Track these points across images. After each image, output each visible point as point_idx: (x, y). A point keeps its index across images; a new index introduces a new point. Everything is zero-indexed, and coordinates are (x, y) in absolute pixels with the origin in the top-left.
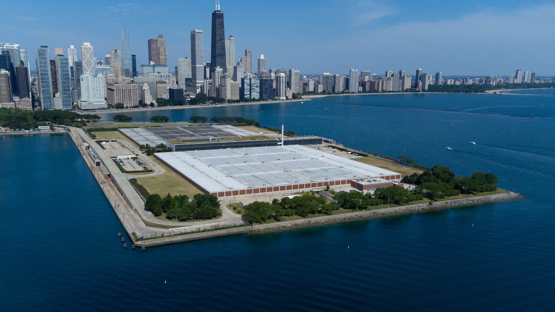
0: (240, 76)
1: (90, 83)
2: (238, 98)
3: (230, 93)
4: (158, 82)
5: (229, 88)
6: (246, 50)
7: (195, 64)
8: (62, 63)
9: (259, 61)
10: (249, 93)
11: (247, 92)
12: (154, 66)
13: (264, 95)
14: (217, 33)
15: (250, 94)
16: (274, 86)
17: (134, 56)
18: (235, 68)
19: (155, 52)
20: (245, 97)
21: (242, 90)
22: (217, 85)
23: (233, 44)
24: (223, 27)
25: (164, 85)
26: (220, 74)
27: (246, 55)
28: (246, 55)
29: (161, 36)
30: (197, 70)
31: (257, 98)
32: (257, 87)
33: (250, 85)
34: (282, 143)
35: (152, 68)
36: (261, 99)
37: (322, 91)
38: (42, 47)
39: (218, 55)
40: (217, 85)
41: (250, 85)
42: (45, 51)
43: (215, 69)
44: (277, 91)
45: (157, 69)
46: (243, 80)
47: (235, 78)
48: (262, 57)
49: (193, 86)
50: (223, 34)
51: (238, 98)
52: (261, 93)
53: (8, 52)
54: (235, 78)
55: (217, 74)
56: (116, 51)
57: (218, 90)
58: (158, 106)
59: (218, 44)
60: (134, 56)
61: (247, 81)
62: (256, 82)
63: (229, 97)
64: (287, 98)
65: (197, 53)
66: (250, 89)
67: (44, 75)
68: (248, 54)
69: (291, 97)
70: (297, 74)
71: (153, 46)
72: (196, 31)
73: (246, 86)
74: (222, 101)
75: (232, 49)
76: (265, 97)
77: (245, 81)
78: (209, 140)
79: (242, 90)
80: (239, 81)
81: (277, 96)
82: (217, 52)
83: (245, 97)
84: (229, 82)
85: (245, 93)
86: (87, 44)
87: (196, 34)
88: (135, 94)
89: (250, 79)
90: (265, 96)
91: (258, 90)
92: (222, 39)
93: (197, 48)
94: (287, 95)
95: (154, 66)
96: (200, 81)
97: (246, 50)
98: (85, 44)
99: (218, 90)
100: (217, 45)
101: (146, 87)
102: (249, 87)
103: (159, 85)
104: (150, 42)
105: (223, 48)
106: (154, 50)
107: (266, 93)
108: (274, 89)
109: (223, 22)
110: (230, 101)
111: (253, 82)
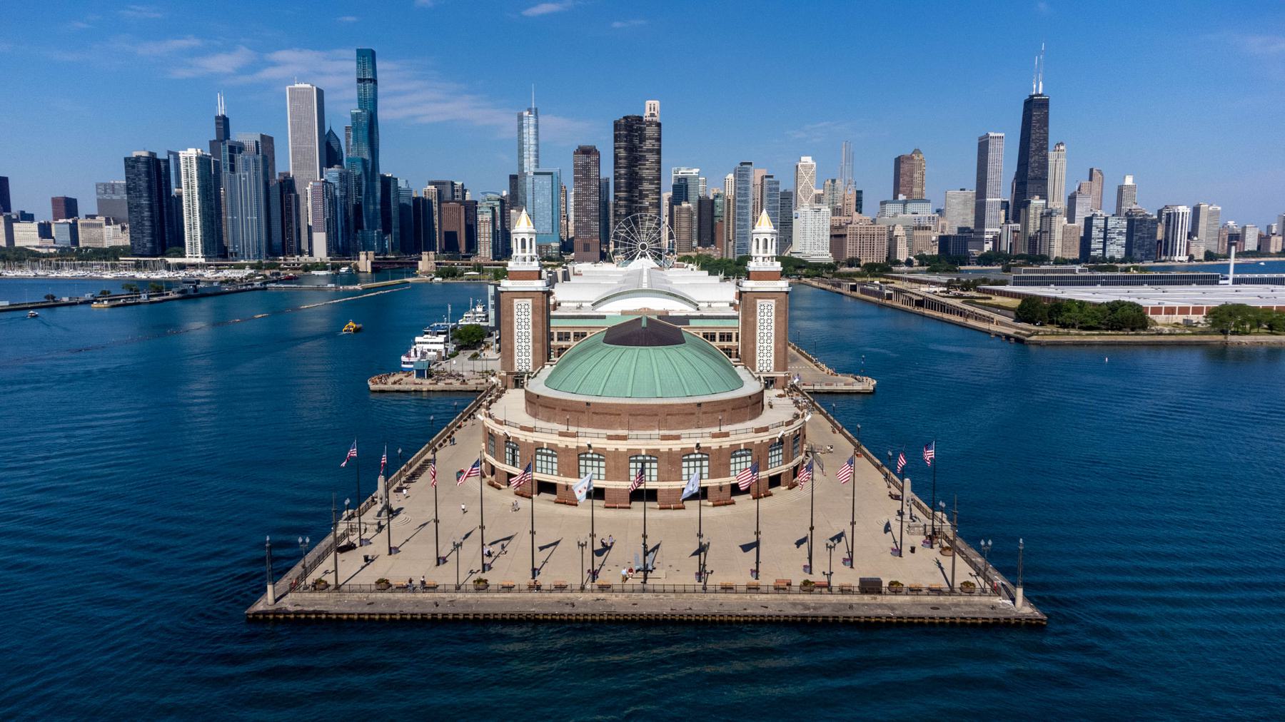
0: (1081, 213)
1: (809, 221)
2: (1077, 256)
3: (1060, 244)
4: (915, 228)
5: (1058, 235)
6: (1091, 170)
7: (985, 197)
8: (770, 189)
9: (1120, 190)
10: (1101, 246)
11: (1096, 245)
12: (905, 203)
13: (1134, 251)
14: (1033, 137)
15: (1104, 249)
16: (1160, 235)
17: (859, 193)
18: (1072, 199)
19: (907, 179)
20: (1093, 253)
21: (1086, 242)
22: (1031, 231)
23: (1063, 160)
24: (1047, 125)
25: (927, 233)
26: (1039, 211)
27: (1091, 179)
28: (1091, 179)
29: (917, 151)
30: (988, 208)
31: (1118, 256)
32: (1120, 233)
33: (1106, 230)
34: (1230, 281)
35: (900, 207)
36: (1129, 257)
37: (1279, 249)
38: (742, 164)
39: (1030, 177)
40: (1031, 231)
41: (1106, 230)
42: (747, 170)
43: (1029, 202)
44: (1167, 244)
45: (910, 207)
46: (1089, 222)
47: (1071, 217)
48: (1129, 181)
49: (977, 240)
50: (1046, 139)
51: (1077, 256)
52: (1129, 246)
53: (686, 179)
54: (1071, 217)
55: (1032, 211)
56: (834, 181)
57: (1033, 242)
58: (606, 479)
59: (1034, 160)
60: (859, 193)
61: (1098, 223)
62: (1119, 225)
63: (1057, 252)
64: (1191, 258)
65: (989, 176)
66: (1105, 238)
67: (742, 208)
68: (1096, 176)
69: (1202, 257)
70: (1213, 214)
71: (905, 167)
72: (992, 134)
73: (1095, 232)
74: (1044, 259)
75: (1062, 169)
76: (1139, 256)
77: (1095, 222)
78: (1073, 271)
79: (1086, 242)
80: (1079, 223)
81: (1166, 254)
82: (1030, 174)
83: (1093, 253)
84: (1060, 222)
85: (1093, 246)
86: (807, 160)
87: (991, 141)
88: (882, 242)
89: (1106, 219)
90: (1137, 253)
91: (1123, 240)
92: (1043, 148)
93: (989, 166)
94: (1192, 251)
95: (905, 203)
96: (990, 231)
97: (1091, 170)
98: (803, 159)
99: (1033, 242)
100: (1032, 160)
101: (899, 231)
102: (1102, 235)
103: (917, 233)
104: (898, 161)
105: (1044, 166)
106: (903, 176)
107: (1139, 248)
108: (1160, 242)
109: (1047, 114)
110: (1058, 261)
111: (1111, 223)
